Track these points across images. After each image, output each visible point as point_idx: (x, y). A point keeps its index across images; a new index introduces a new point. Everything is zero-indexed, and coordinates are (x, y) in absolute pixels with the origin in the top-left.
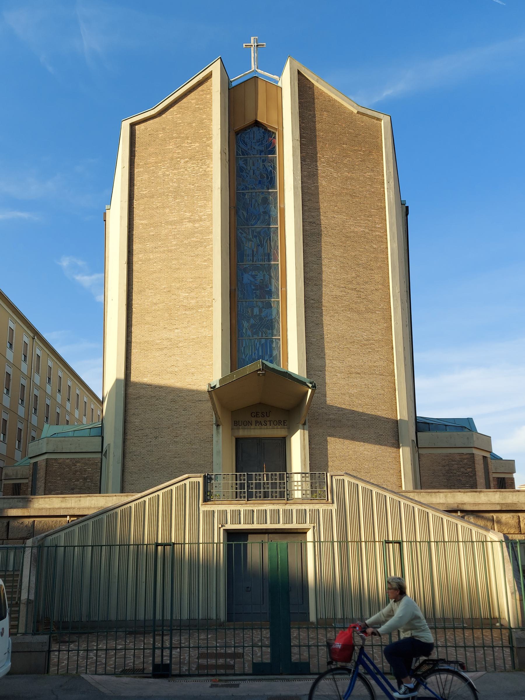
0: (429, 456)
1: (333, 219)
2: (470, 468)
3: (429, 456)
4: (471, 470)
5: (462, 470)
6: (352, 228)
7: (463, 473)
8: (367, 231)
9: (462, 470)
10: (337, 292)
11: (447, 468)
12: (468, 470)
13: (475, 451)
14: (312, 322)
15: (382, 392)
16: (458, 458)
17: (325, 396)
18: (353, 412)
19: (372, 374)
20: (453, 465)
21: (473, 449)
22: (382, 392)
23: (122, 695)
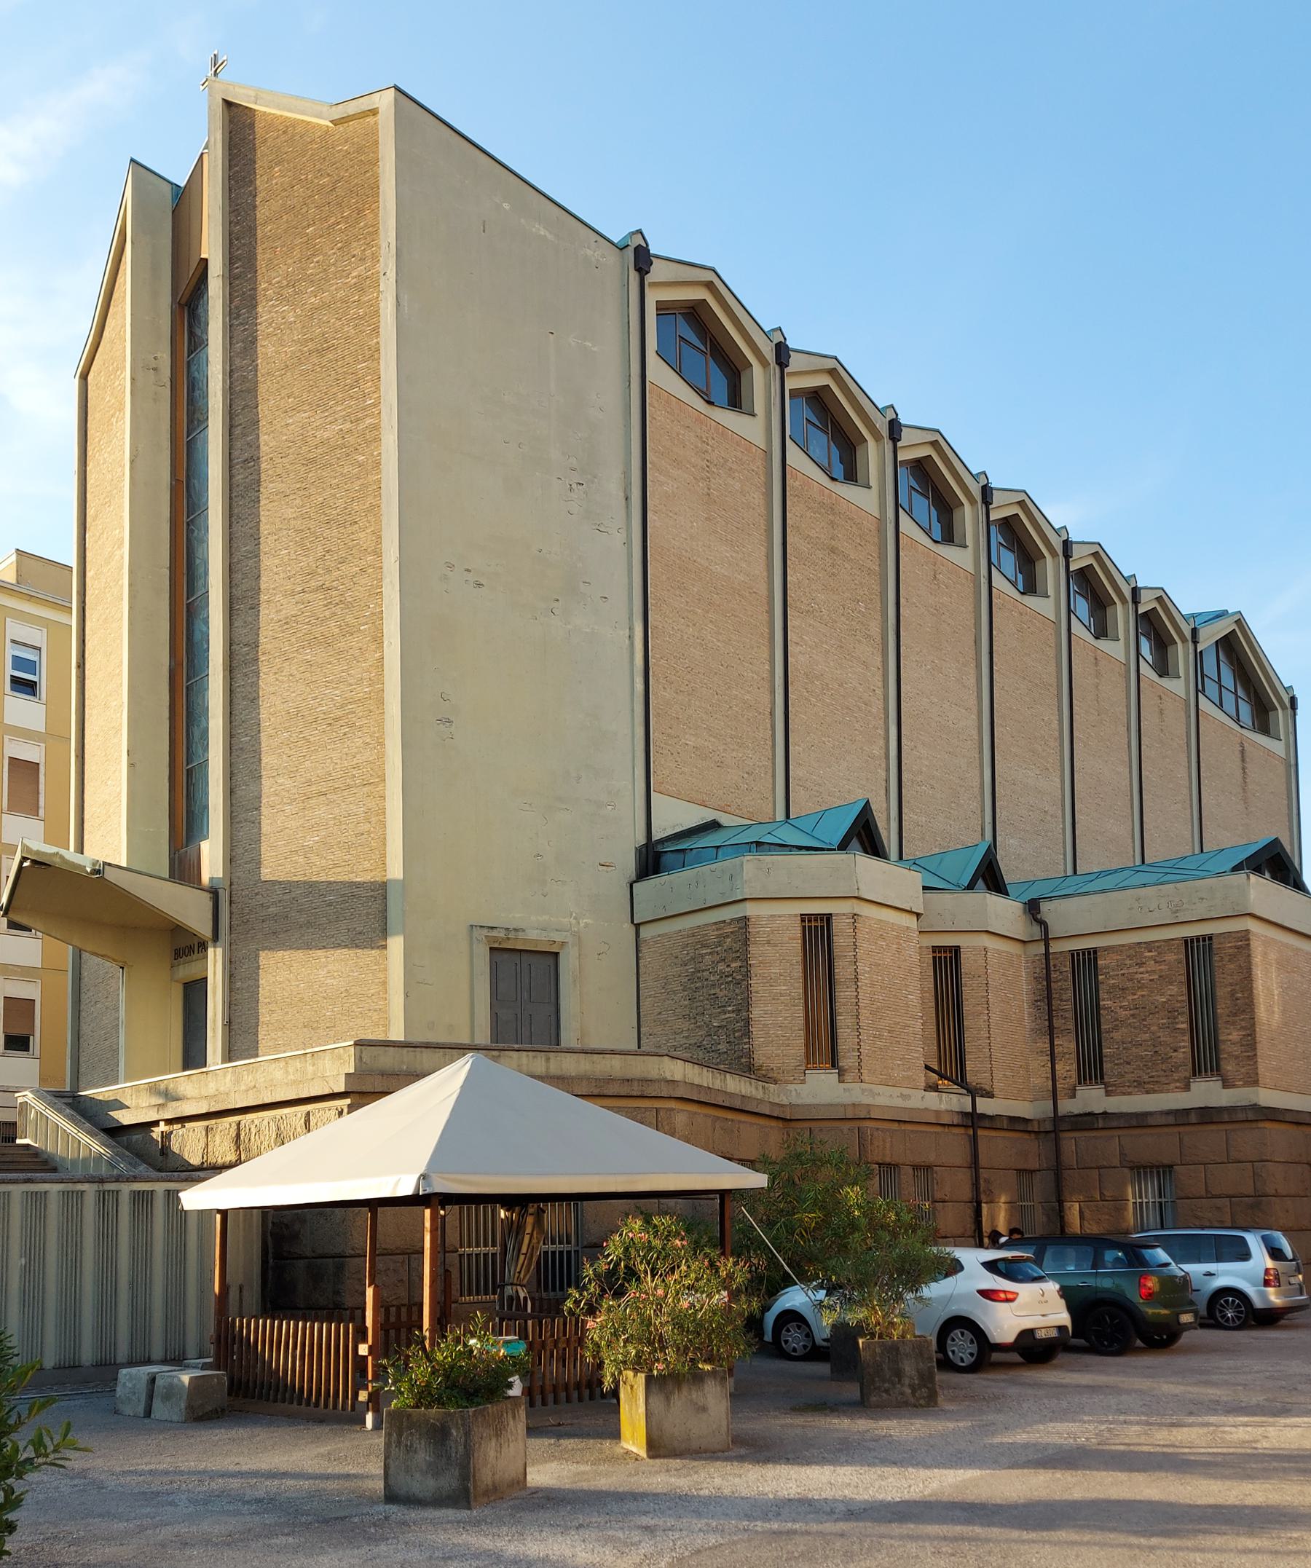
0: (656, 942)
1: (285, 431)
2: (734, 960)
3: (656, 942)
4: (738, 964)
5: (721, 966)
6: (318, 434)
7: (722, 974)
8: (348, 426)
9: (721, 966)
10: (290, 609)
11: (691, 968)
12: (733, 965)
13: (750, 910)
14: (244, 699)
15: (367, 827)
16: (713, 936)
17: (259, 864)
18: (311, 887)
19: (349, 787)
20: (702, 956)
21: (748, 905)
22: (367, 827)
23: (552, 1441)
